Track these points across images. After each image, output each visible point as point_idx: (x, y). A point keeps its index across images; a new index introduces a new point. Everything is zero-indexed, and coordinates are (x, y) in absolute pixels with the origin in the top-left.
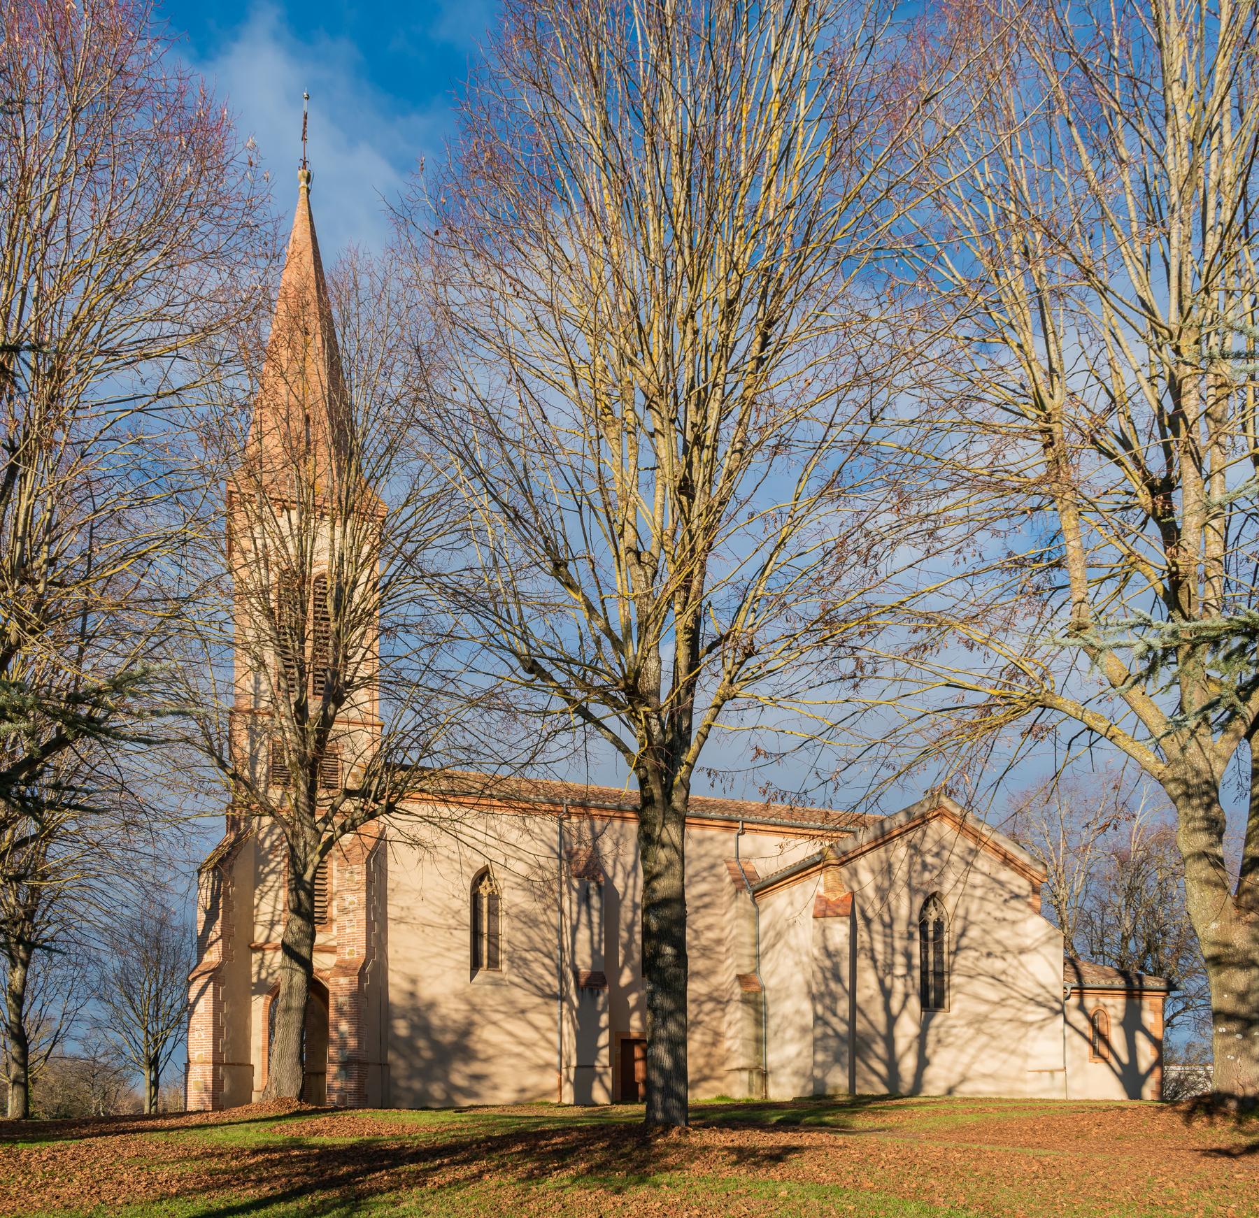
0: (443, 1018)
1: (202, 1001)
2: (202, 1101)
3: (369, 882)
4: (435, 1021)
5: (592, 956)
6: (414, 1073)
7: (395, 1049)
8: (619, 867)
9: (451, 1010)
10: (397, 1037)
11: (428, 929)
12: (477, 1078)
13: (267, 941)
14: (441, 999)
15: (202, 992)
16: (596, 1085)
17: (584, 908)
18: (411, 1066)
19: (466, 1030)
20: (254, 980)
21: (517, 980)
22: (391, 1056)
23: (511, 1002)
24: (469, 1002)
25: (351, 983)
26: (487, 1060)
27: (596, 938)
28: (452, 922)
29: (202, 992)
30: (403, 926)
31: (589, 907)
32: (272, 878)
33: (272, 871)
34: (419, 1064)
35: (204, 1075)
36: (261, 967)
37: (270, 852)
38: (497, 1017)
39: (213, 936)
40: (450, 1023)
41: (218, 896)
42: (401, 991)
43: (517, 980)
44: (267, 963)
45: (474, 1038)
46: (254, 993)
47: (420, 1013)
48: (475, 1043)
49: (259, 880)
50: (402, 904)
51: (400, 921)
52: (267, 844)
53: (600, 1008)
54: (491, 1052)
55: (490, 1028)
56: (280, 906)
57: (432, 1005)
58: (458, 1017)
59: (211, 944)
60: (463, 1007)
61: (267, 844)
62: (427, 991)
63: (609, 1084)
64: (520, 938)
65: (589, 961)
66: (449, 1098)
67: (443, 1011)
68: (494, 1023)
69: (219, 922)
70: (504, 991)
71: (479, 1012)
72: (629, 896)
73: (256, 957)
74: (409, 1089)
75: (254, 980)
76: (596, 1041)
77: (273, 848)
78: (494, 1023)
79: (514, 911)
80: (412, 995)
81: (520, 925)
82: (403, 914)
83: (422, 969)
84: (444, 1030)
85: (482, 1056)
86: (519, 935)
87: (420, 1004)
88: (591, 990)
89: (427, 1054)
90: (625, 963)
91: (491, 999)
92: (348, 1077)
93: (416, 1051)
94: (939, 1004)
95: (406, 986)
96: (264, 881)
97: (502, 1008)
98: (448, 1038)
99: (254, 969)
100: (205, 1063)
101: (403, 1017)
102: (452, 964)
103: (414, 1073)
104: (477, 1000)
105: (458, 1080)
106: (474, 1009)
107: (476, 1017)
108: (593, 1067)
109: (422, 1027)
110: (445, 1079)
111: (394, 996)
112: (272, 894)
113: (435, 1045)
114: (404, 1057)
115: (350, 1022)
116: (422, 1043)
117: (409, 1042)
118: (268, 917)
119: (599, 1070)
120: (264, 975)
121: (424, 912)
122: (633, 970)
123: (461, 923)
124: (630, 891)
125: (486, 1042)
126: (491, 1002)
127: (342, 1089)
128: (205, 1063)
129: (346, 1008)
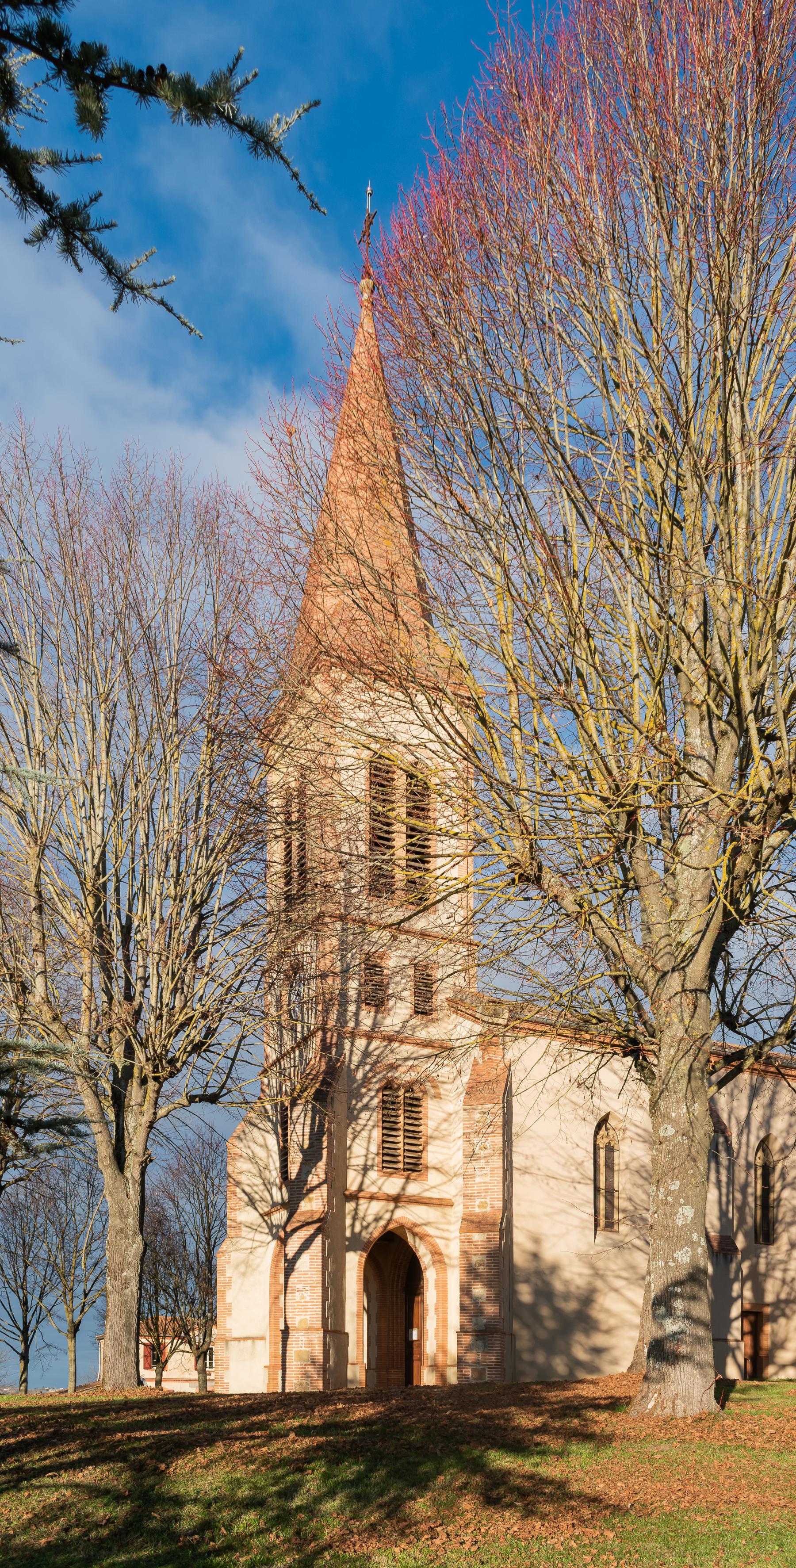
0: (566, 1283)
1: (305, 1257)
2: (306, 1375)
3: (504, 1124)
4: (558, 1286)
5: (720, 1219)
6: (538, 1344)
7: (520, 1318)
8: (733, 1121)
9: (573, 1275)
10: (521, 1304)
11: (552, 1182)
12: (597, 1351)
13: (360, 1189)
14: (564, 1262)
15: (306, 1245)
16: (730, 1361)
17: (713, 1165)
18: (534, 1337)
19: (588, 1299)
20: (348, 1234)
21: (638, 1242)
22: (516, 1326)
23: (632, 1267)
24: (593, 1267)
25: (489, 1240)
26: (608, 1331)
27: (724, 1199)
28: (576, 1175)
29: (306, 1245)
30: (527, 1176)
31: (718, 1163)
32: (365, 1115)
33: (366, 1107)
34: (543, 1335)
35: (310, 1343)
36: (354, 1219)
37: (362, 1085)
38: (619, 1283)
39: (313, 1180)
40: (573, 1289)
41: (321, 1133)
42: (524, 1251)
43: (638, 1242)
44: (361, 1214)
45: (596, 1306)
46: (349, 1249)
47: (543, 1276)
48: (595, 1313)
49: (352, 1117)
50: (527, 1152)
51: (525, 1171)
52: (360, 1075)
53: (732, 1275)
54: (612, 1322)
55: (612, 1295)
56: (374, 1149)
57: (554, 1269)
58: (581, 1282)
59: (311, 1190)
60: (587, 1271)
61: (360, 1075)
62: (550, 1253)
63: (741, 1360)
64: (640, 1195)
65: (717, 1223)
66: (571, 1373)
67: (567, 1274)
68: (616, 1290)
69: (322, 1165)
70: (626, 1254)
71: (602, 1277)
72: (743, 1154)
73: (350, 1206)
74: (533, 1364)
75: (348, 1234)
76: (729, 1311)
77: (366, 1080)
78: (616, 1290)
79: (634, 1165)
80: (535, 1256)
81: (641, 1182)
82: (528, 1163)
83: (545, 1228)
84: (567, 1297)
85: (604, 1327)
86: (640, 1192)
87: (543, 1266)
88: (725, 1255)
89: (551, 1324)
90: (740, 1226)
91: (614, 1264)
92: (487, 1348)
93: (539, 1319)
94: (213, 1321)
95: (530, 1246)
96: (356, 1118)
97: (624, 1274)
98: (571, 1306)
99: (348, 1221)
100: (310, 1329)
101: (527, 1281)
102: (576, 1222)
103: (538, 1344)
104: (600, 1264)
105: (581, 1354)
106: (597, 1274)
107: (599, 1284)
108: (726, 1340)
109: (544, 1293)
110: (567, 1353)
111: (519, 1258)
112: (365, 1134)
113: (557, 1312)
114: (526, 1326)
115: (489, 1284)
116: (545, 1311)
117: (532, 1309)
118: (361, 1161)
119: (733, 1344)
120: (357, 1229)
121: (549, 1163)
122: (746, 1235)
123: (585, 1177)
124: (744, 1149)
125: (607, 1311)
126: (613, 1266)
127: (477, 1362)
128: (310, 1329)
129: (482, 1269)
